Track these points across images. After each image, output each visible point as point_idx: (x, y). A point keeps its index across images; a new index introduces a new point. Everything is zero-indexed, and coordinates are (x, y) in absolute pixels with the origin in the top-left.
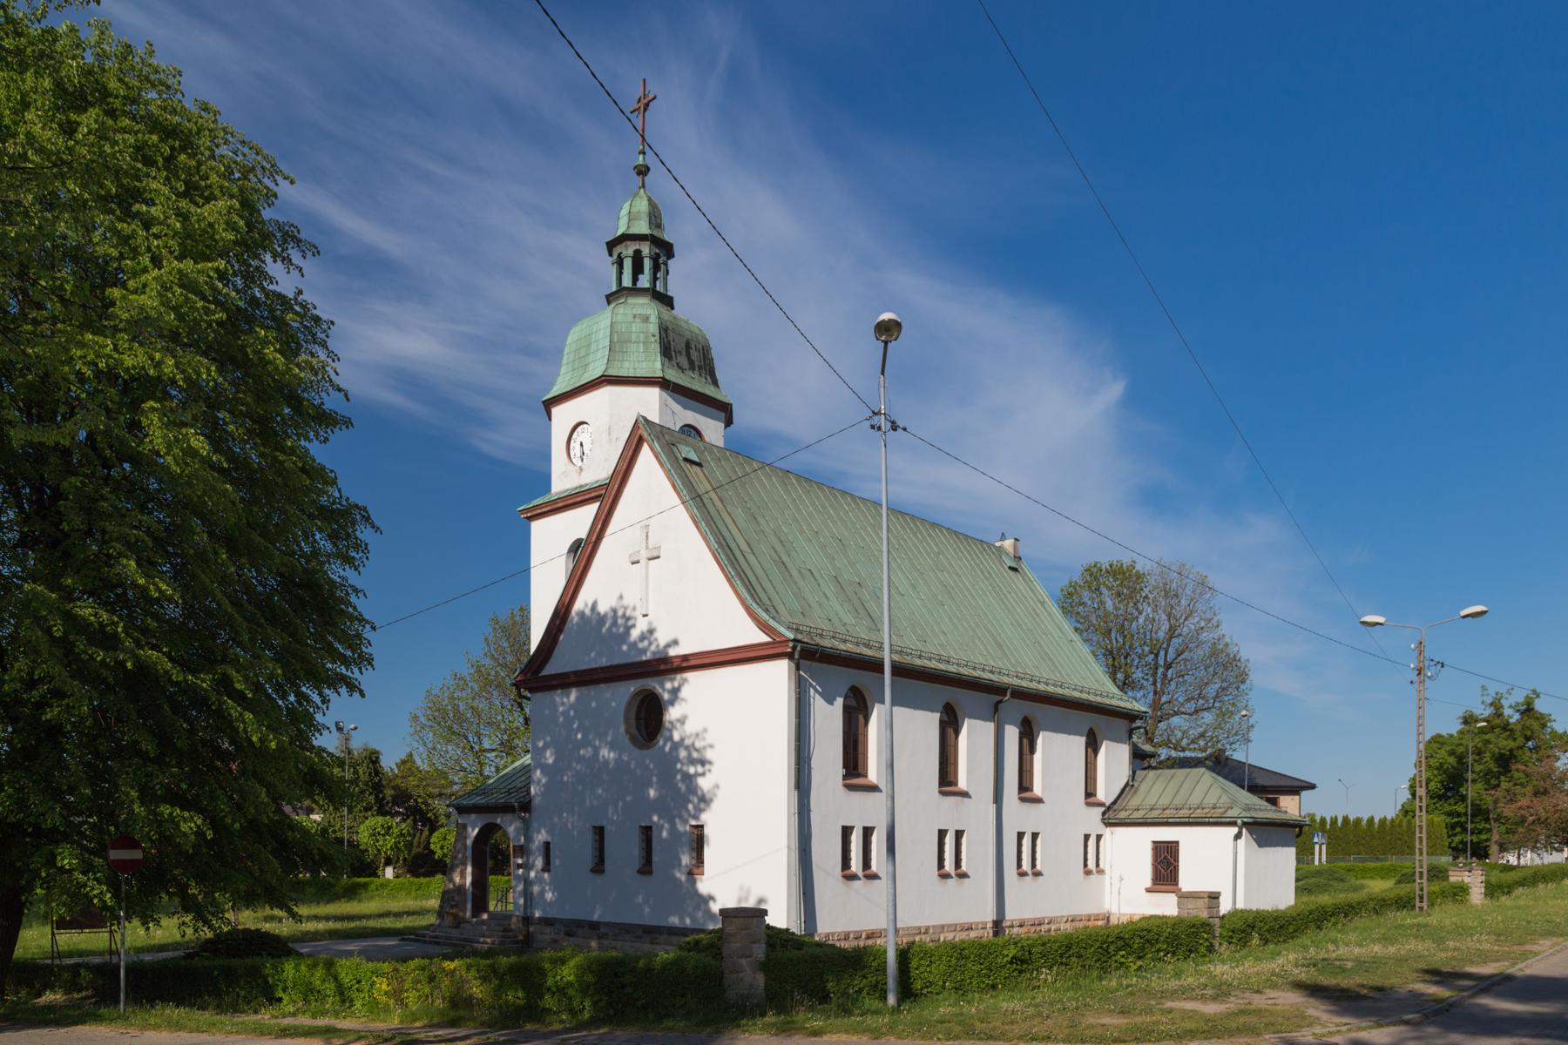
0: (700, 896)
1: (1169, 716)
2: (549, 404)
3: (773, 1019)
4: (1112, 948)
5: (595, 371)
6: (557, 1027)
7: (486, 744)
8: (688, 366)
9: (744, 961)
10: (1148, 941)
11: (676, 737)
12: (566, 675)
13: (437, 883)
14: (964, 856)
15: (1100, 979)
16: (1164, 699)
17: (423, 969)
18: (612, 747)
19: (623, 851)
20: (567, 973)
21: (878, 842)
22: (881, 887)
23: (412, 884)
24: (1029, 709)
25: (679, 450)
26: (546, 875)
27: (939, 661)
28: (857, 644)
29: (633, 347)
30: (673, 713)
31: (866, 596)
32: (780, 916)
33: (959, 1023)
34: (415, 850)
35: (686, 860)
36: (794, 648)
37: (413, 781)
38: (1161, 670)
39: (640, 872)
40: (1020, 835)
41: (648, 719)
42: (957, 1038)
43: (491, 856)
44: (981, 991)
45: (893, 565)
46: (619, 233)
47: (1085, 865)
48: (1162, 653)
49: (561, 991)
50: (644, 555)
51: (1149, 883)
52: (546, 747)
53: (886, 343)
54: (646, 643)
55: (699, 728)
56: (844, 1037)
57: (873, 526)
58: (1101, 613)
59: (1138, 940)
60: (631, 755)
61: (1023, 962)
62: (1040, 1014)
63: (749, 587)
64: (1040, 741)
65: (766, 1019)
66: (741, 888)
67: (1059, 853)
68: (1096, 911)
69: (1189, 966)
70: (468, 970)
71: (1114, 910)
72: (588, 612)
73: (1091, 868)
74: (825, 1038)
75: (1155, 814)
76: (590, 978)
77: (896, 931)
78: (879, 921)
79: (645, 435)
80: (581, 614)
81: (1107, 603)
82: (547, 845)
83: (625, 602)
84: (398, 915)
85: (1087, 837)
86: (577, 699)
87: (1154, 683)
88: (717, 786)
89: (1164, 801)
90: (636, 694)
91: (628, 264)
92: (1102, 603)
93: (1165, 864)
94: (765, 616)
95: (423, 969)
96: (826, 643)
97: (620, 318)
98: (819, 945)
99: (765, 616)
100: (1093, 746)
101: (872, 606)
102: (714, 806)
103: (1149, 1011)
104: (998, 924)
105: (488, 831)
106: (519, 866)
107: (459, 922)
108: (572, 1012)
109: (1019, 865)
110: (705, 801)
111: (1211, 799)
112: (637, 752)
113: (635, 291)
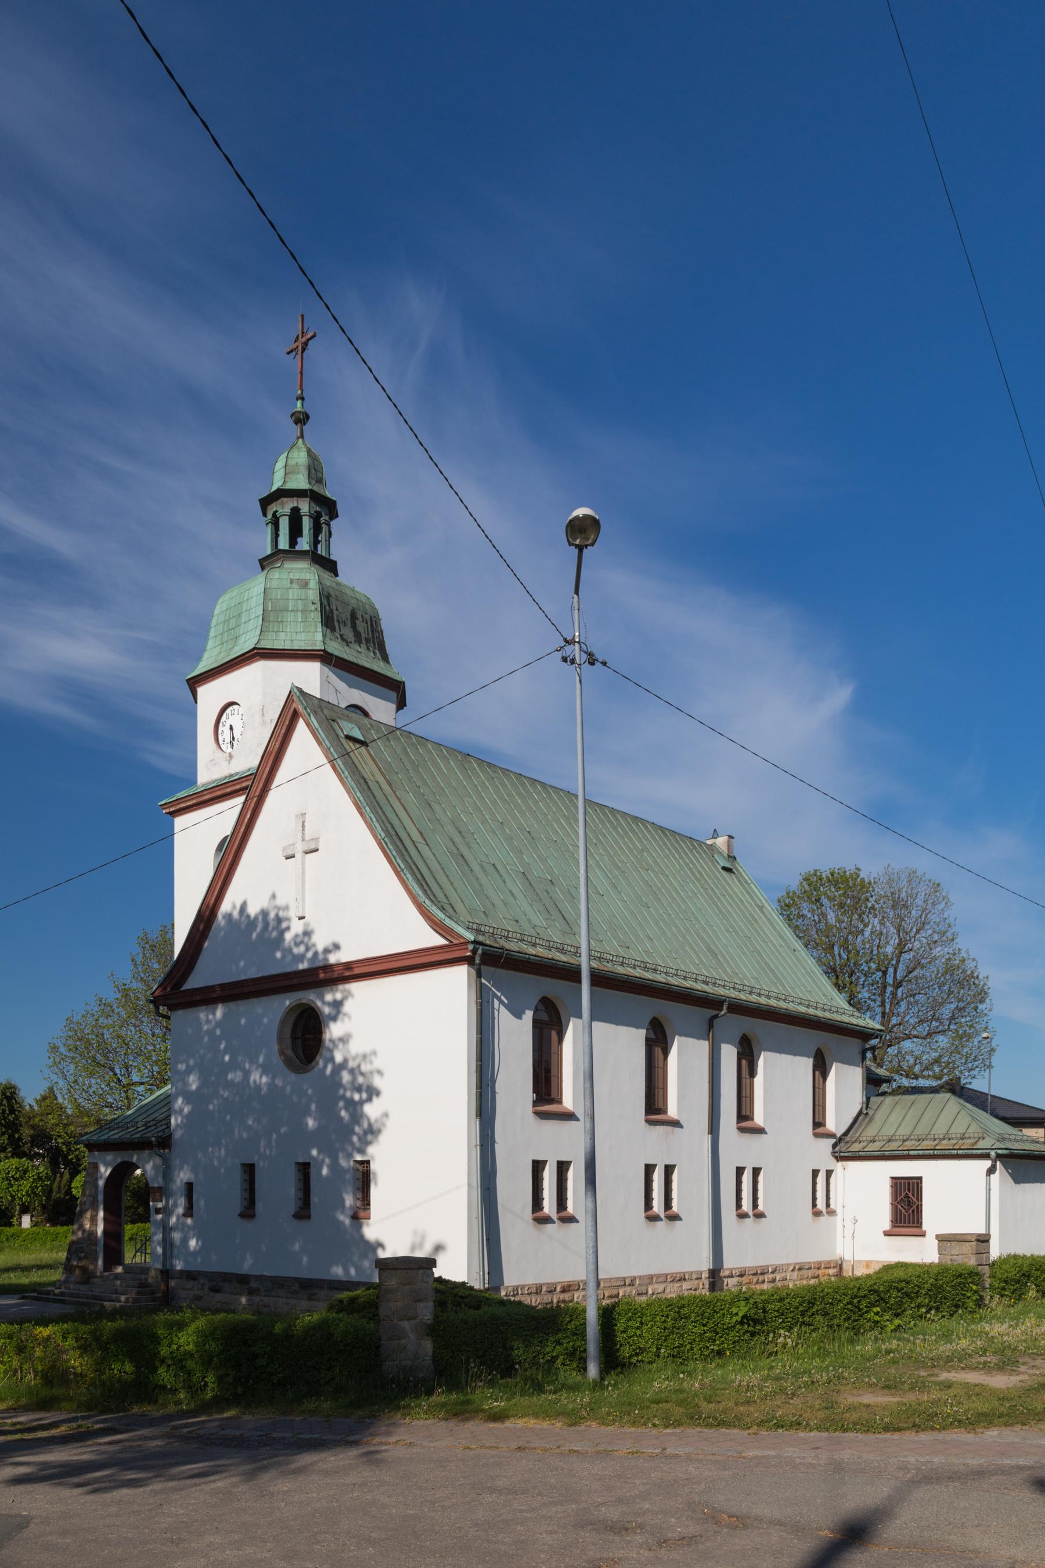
0: (367, 1243)
1: (899, 1040)
2: (194, 683)
3: (443, 1398)
4: (864, 1304)
5: (246, 644)
6: (172, 1408)
7: (135, 1078)
8: (353, 641)
9: (406, 1325)
10: (907, 1294)
11: (339, 1058)
12: (210, 989)
13: (67, 1234)
14: (675, 1195)
15: (851, 1341)
16: (894, 1020)
17: (10, 1337)
18: (265, 1071)
19: (277, 1192)
20: (186, 1340)
21: (575, 1178)
22: (578, 1232)
23: (47, 1233)
24: (749, 1026)
25: (349, 745)
26: (189, 1221)
27: (645, 969)
28: (549, 948)
29: (290, 617)
30: (334, 1030)
31: (559, 894)
32: (456, 1267)
33: (681, 1403)
34: (55, 1195)
35: (349, 1200)
36: (474, 951)
37: (52, 1120)
38: (889, 989)
39: (242, 1215)
40: (740, 1171)
41: (306, 1037)
42: (678, 1424)
43: (130, 1201)
44: (705, 1359)
45: (590, 861)
46: (275, 488)
47: (814, 1205)
48: (891, 970)
49: (180, 1362)
50: (300, 847)
51: (887, 1225)
52: (189, 1071)
53: (581, 549)
54: (302, 948)
55: (367, 1049)
56: (532, 1422)
57: (567, 819)
58: (822, 926)
59: (894, 1294)
60: (287, 1080)
61: (756, 1322)
62: (783, 1391)
63: (422, 882)
64: (761, 1063)
65: (434, 1398)
66: (415, 1233)
67: (782, 1191)
68: (826, 1258)
69: (958, 1325)
70: (65, 1338)
71: (848, 1257)
72: (236, 914)
73: (821, 1208)
74: (508, 1424)
75: (894, 1145)
76: (212, 1346)
77: (598, 1283)
78: (575, 1270)
79: (300, 709)
80: (229, 916)
81: (830, 910)
82: (189, 1187)
83: (280, 901)
84: (26, 1269)
85: (815, 1173)
86: (225, 1016)
87: (883, 1004)
88: (386, 1115)
89: (904, 1131)
90: (291, 1009)
91: (284, 524)
92: (824, 915)
93: (907, 1206)
94: (440, 915)
95: (10, 1337)
96: (513, 946)
97: (274, 584)
98: (502, 1303)
99: (440, 915)
100: (821, 1069)
101: (566, 907)
102: (383, 1138)
103: (919, 1386)
104: (715, 1275)
105: (122, 1172)
106: (158, 1211)
107: (88, 1277)
108: (190, 1388)
109: (739, 1205)
110: (372, 1132)
111: (958, 1129)
112: (293, 1077)
113: (293, 553)
